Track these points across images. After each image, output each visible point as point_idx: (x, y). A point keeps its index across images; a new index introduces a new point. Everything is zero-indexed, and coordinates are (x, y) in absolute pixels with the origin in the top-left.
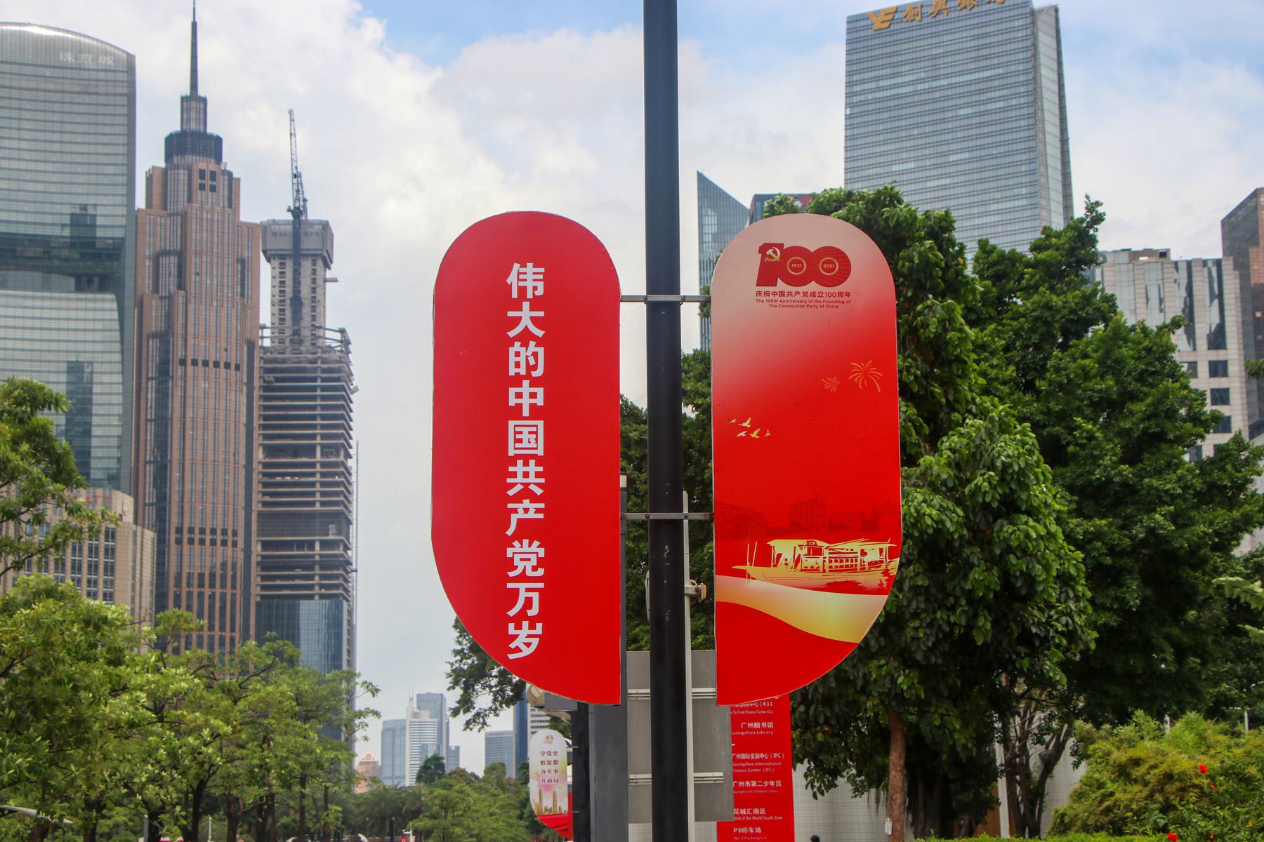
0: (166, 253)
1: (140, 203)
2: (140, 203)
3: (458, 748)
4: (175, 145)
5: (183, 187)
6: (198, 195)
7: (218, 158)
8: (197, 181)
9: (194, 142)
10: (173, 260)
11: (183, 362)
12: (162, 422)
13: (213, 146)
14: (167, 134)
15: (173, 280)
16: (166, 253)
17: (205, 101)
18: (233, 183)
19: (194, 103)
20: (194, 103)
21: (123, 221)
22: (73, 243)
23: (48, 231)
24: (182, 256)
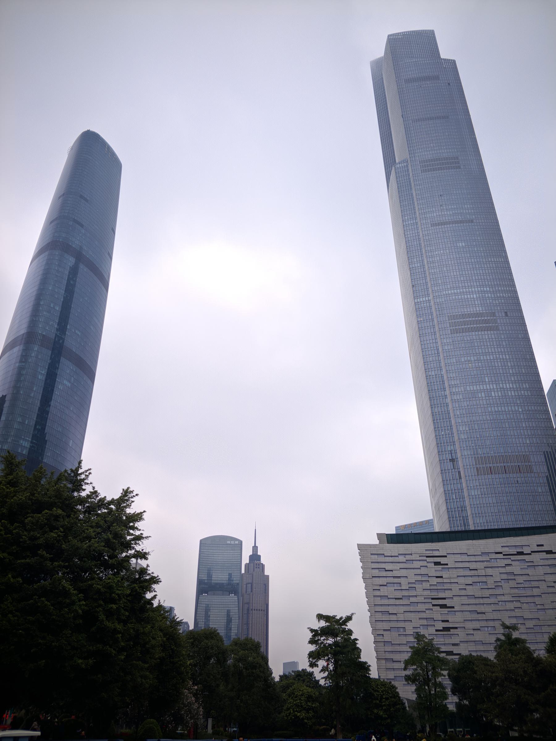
0: (249, 583)
1: (243, 571)
2: (243, 571)
3: (320, 617)
4: (251, 557)
5: (252, 568)
6: (255, 569)
7: (260, 560)
8: (255, 566)
9: (255, 557)
10: (250, 585)
11: (252, 610)
12: (248, 624)
13: (259, 558)
14: (92, 129)
15: (250, 590)
16: (249, 583)
17: (257, 547)
18: (263, 566)
19: (255, 548)
20: (255, 548)
21: (239, 579)
22: (229, 584)
23: (223, 582)
24: (252, 584)
